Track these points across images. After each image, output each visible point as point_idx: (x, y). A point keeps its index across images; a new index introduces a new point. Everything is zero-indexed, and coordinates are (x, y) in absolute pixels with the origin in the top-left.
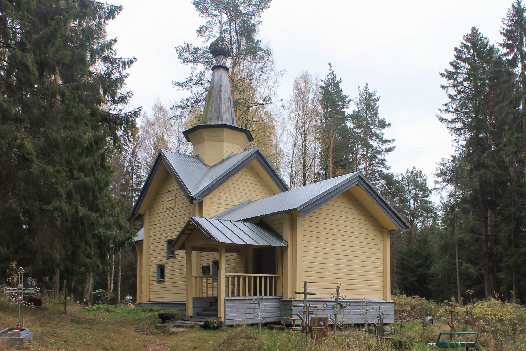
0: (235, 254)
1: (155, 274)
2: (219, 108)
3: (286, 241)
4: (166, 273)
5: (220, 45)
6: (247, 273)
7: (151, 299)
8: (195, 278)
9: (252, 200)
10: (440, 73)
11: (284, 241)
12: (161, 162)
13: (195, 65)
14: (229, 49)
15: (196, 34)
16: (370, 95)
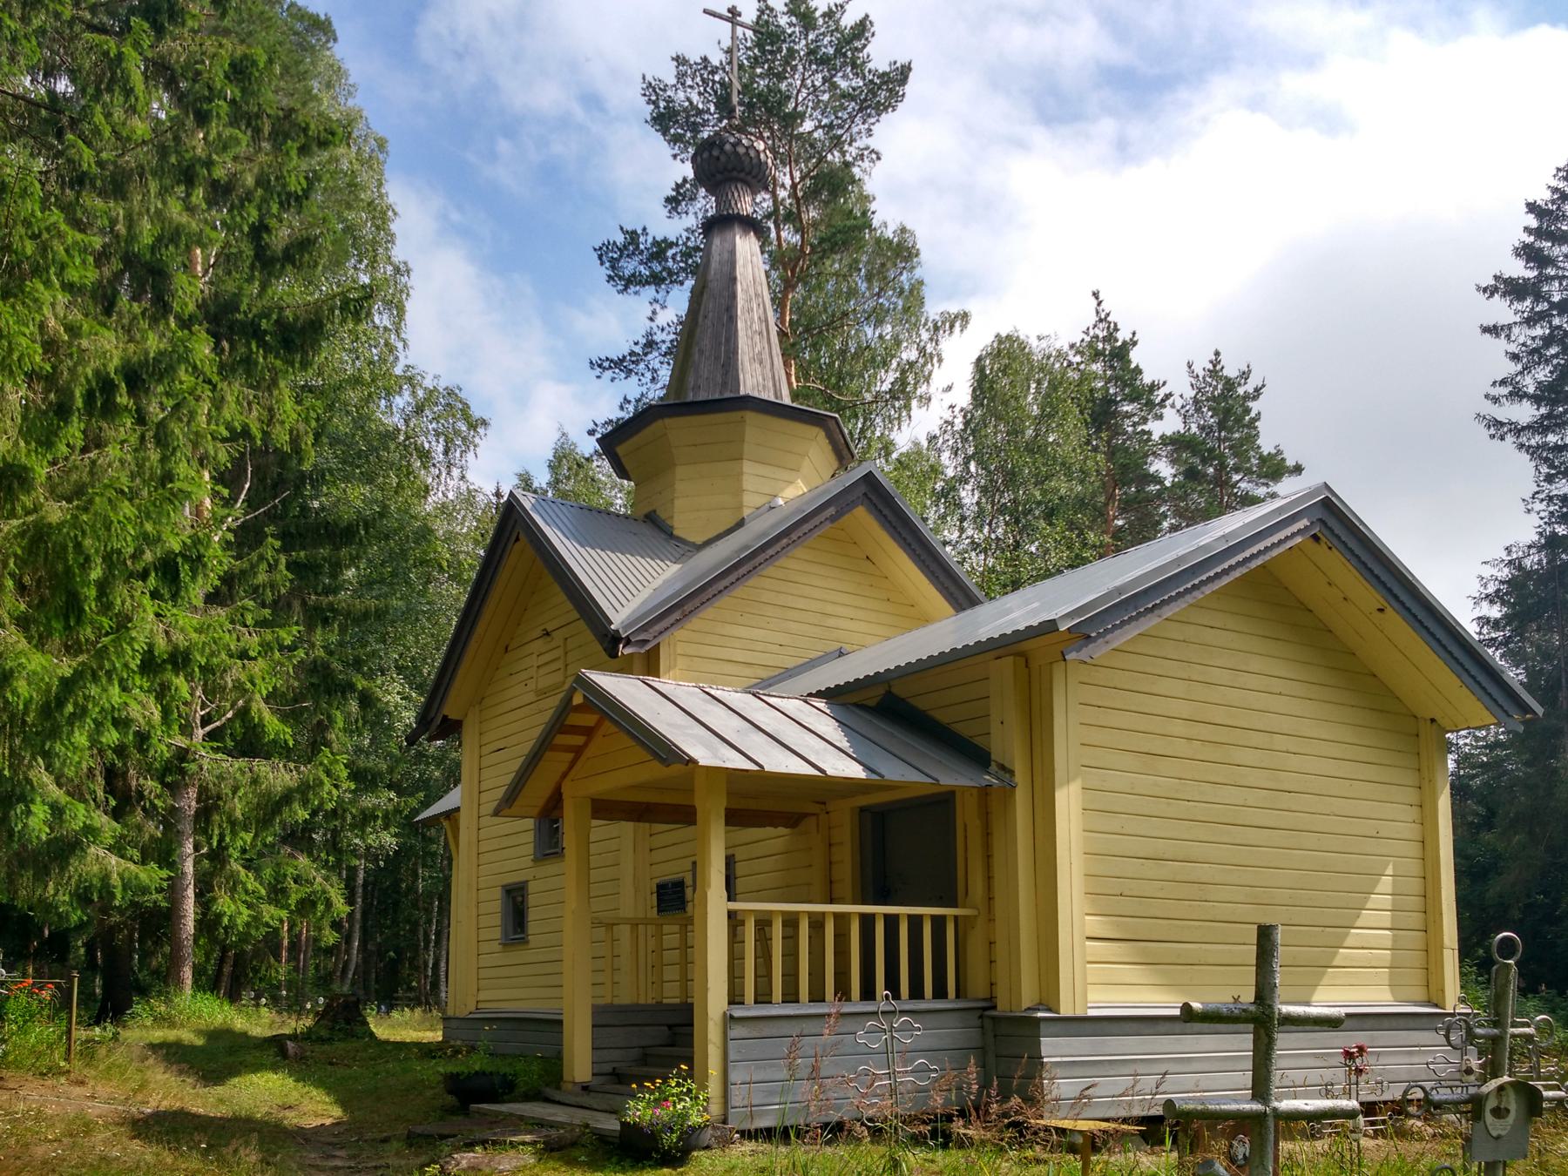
0: (782, 830)
1: (497, 920)
2: (727, 352)
3: (1003, 767)
4: (532, 915)
5: (728, 147)
6: (831, 902)
7: (480, 1006)
8: (628, 927)
9: (847, 648)
10: (1479, 288)
11: (993, 768)
12: (514, 537)
13: (662, 293)
14: (762, 156)
15: (665, 212)
16: (1230, 385)
